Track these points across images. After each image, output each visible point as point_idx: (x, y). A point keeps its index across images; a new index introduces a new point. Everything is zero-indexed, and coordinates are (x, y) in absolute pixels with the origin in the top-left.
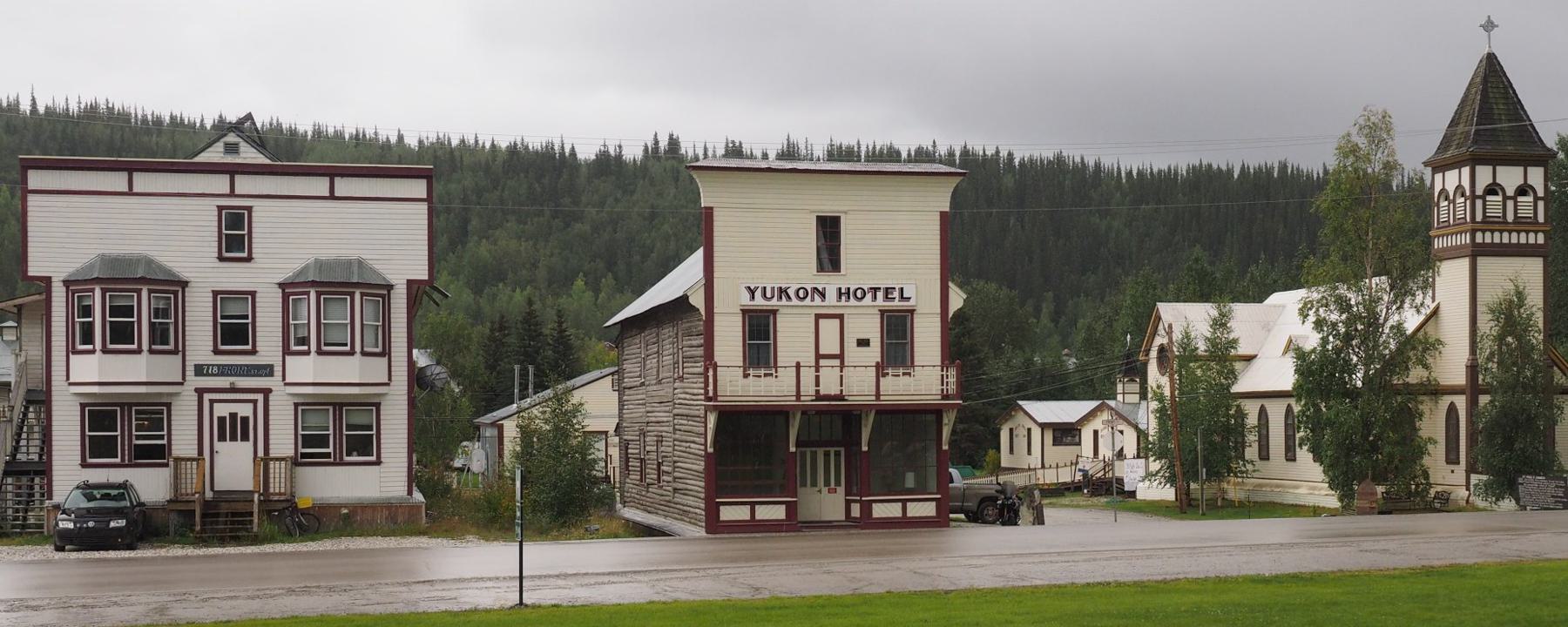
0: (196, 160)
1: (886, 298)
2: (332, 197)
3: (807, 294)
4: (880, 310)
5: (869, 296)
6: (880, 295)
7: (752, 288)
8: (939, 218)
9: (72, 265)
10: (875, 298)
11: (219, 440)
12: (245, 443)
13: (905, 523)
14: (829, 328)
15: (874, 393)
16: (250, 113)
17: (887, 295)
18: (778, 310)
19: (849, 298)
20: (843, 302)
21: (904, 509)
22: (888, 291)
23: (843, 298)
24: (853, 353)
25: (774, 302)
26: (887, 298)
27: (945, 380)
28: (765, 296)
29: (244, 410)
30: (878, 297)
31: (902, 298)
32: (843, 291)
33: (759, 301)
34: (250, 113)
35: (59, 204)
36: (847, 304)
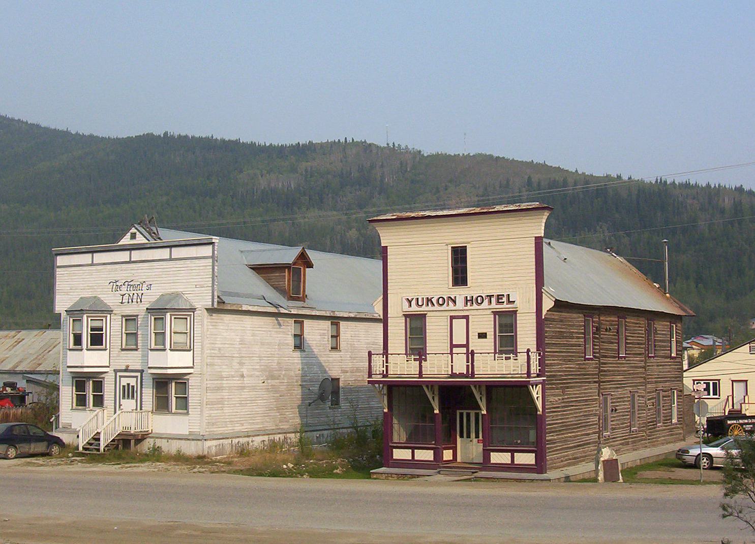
0: (119, 243)
1: (498, 302)
2: (171, 259)
3: (444, 302)
5: (486, 302)
6: (493, 300)
7: (410, 299)
8: (534, 242)
11: (123, 399)
12: (133, 400)
14: (459, 325)
15: (418, 373)
17: (498, 301)
19: (472, 303)
20: (469, 307)
21: (513, 458)
22: (499, 297)
23: (469, 303)
25: (424, 308)
26: (498, 302)
27: (385, 364)
28: (477, 302)
29: (132, 382)
30: (492, 301)
31: (509, 302)
32: (469, 299)
33: (414, 308)
35: (154, 265)
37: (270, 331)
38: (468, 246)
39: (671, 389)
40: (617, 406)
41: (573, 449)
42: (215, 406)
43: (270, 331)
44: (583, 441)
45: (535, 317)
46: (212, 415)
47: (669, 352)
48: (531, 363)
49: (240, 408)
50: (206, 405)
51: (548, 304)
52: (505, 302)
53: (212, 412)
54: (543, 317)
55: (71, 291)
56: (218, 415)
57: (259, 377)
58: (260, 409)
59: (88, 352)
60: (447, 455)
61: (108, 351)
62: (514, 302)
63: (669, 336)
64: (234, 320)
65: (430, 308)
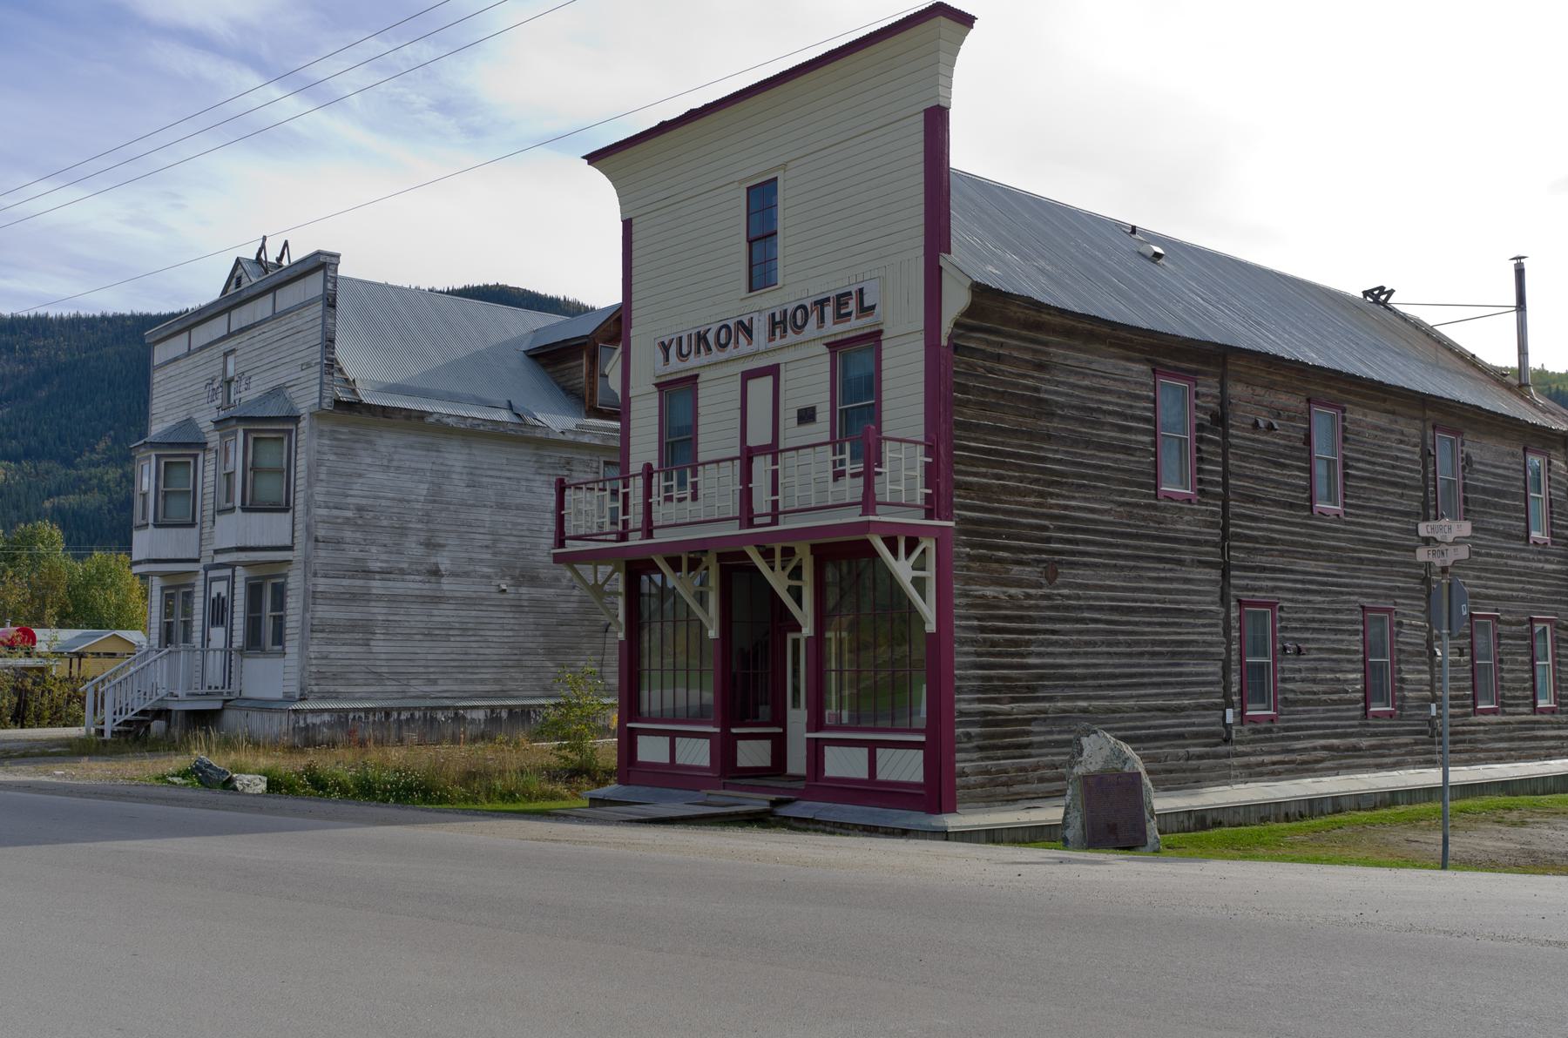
1: (841, 317)
3: (730, 339)
4: (827, 345)
5: (813, 319)
6: (829, 310)
9: (1366, 370)
10: (822, 319)
11: (794, 707)
13: (872, 792)
16: (337, 256)
18: (696, 376)
19: (785, 331)
20: (778, 342)
22: (842, 299)
24: (792, 434)
25: (693, 361)
28: (795, 322)
31: (865, 310)
34: (337, 256)
36: (785, 342)
37: (527, 480)
38: (780, 174)
39: (1531, 619)
40: (1307, 640)
41: (1146, 745)
42: (342, 636)
43: (527, 480)
44: (1149, 728)
45: (921, 345)
46: (332, 656)
47: (1523, 524)
48: (1207, 570)
49: (426, 644)
50: (312, 631)
51: (955, 302)
52: (854, 315)
53: (332, 649)
54: (944, 342)
55: (167, 413)
56: (353, 656)
57: (489, 577)
58: (494, 651)
59: (159, 530)
60: (752, 754)
61: (198, 527)
62: (873, 307)
63: (1521, 484)
64: (412, 447)
65: (704, 359)
